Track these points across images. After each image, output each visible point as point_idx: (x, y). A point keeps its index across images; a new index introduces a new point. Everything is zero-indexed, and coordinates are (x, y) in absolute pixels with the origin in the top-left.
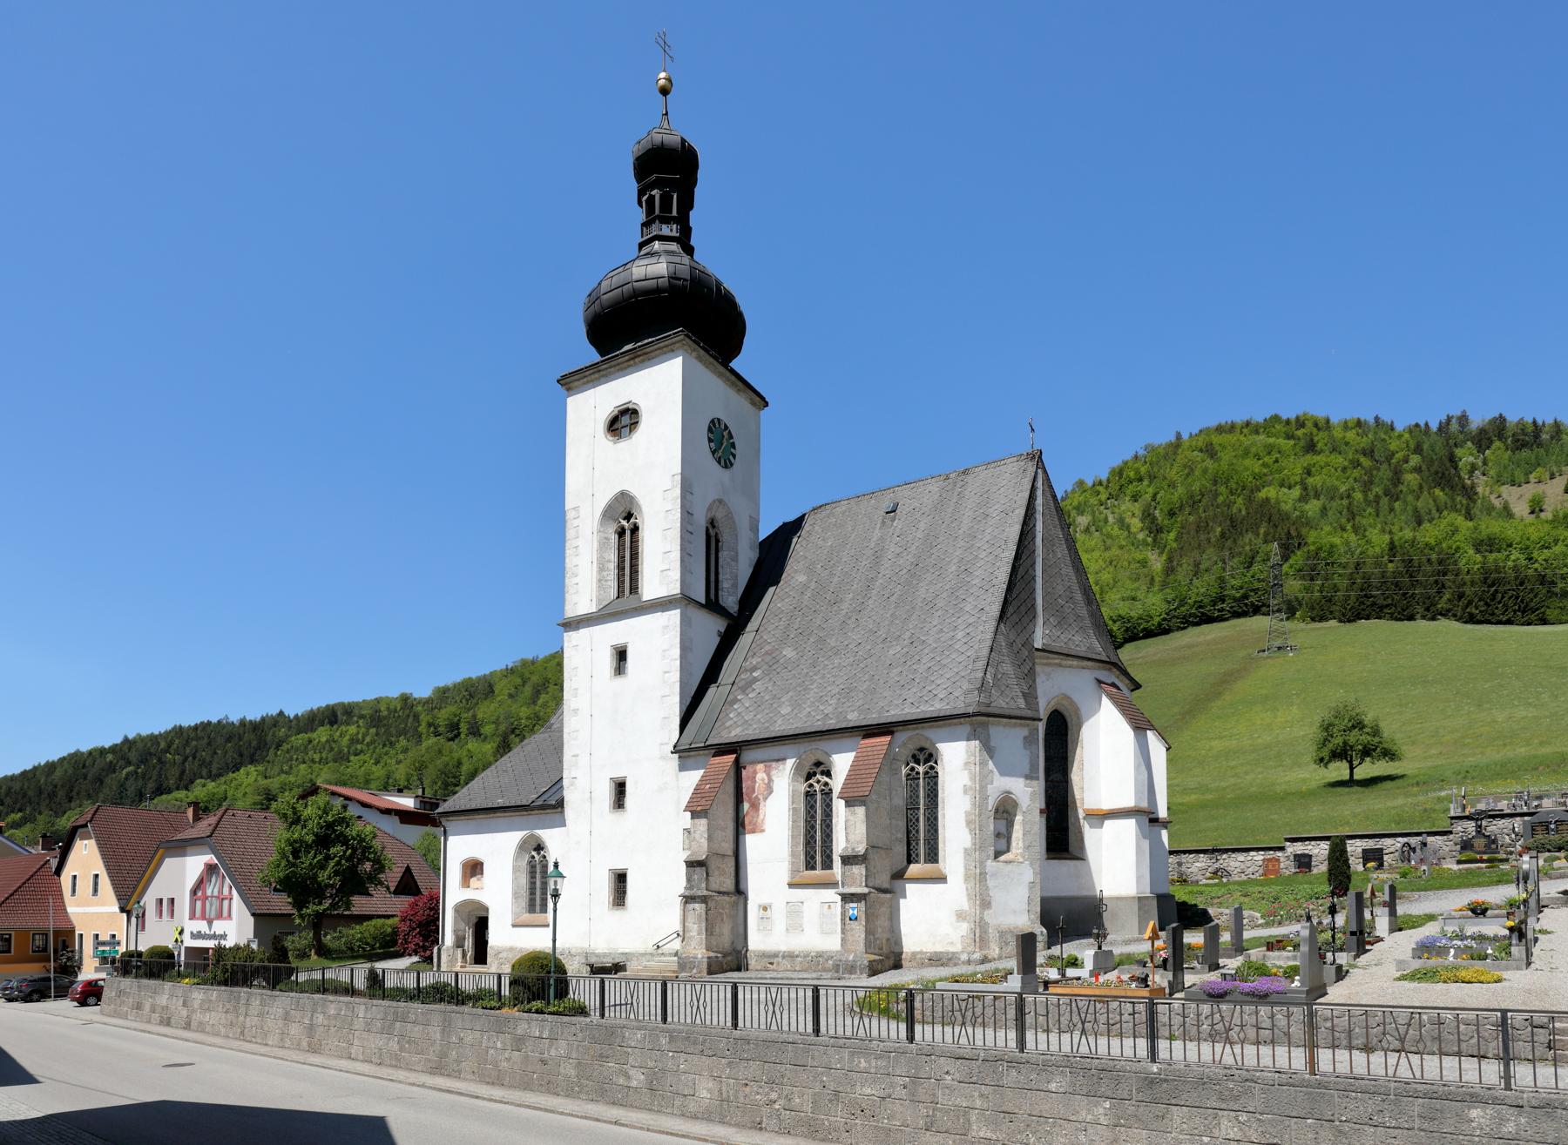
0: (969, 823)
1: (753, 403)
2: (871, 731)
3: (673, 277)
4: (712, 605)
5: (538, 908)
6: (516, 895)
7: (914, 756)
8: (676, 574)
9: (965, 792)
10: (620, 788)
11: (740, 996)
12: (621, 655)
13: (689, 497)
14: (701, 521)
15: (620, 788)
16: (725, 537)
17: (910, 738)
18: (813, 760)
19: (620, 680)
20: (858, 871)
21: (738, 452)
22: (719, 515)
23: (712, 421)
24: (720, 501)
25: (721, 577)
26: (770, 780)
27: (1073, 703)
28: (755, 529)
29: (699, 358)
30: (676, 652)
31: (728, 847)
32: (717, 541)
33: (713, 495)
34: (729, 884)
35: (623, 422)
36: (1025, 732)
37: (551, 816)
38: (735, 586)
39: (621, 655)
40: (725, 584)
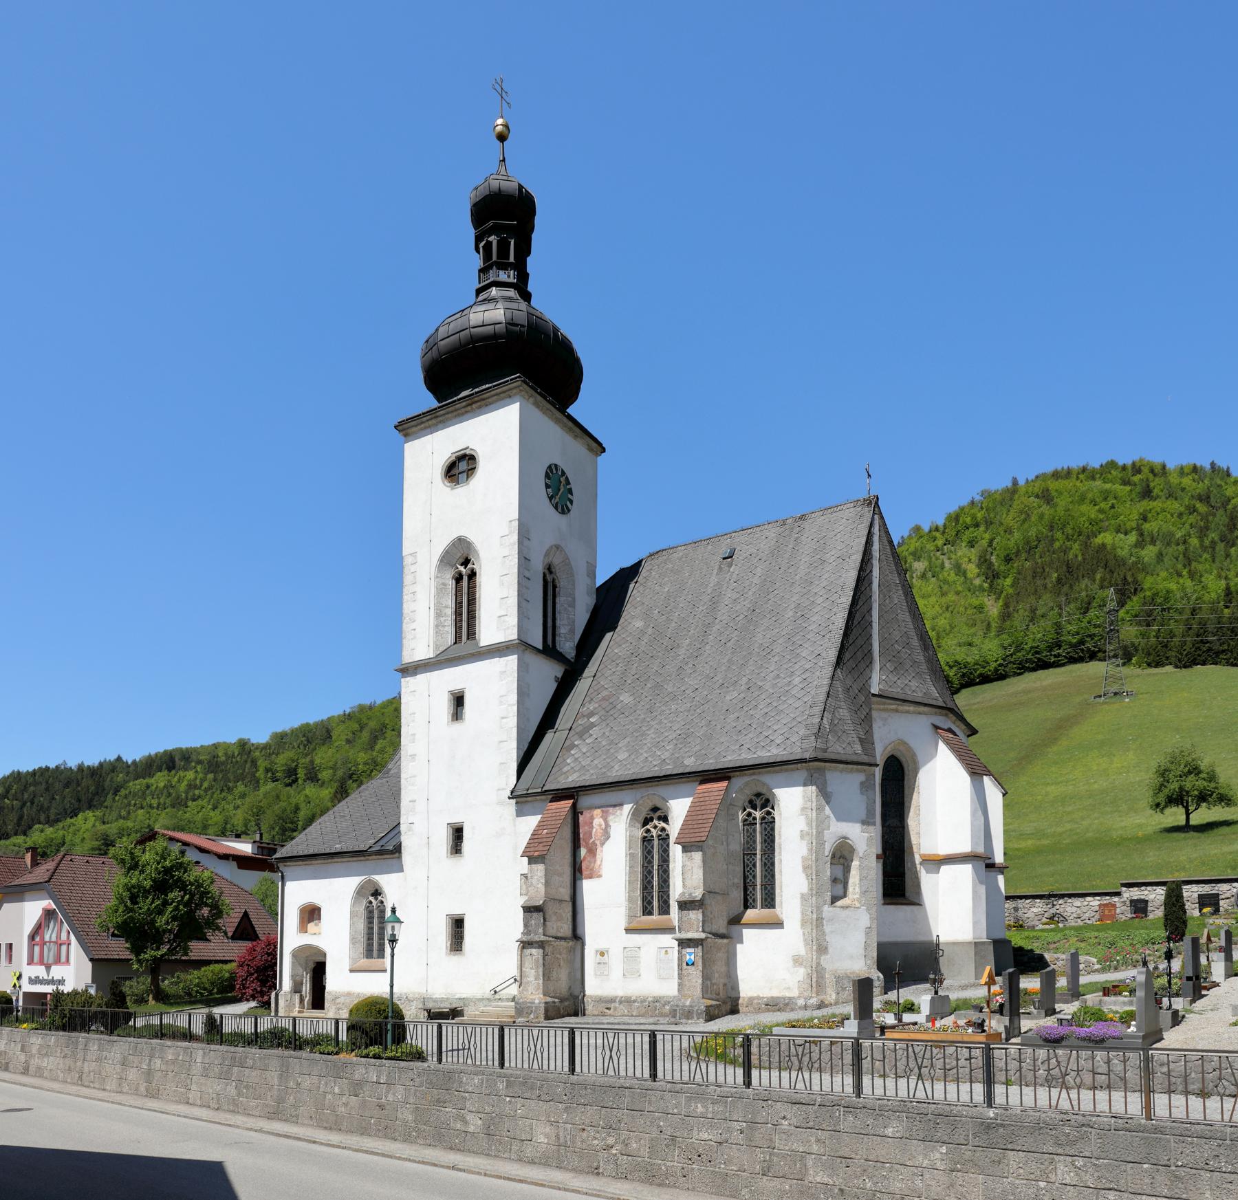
1: (590, 449)
3: (510, 323)
4: (550, 650)
7: (751, 802)
8: (513, 620)
9: (802, 837)
10: (457, 834)
13: (526, 542)
15: (457, 834)
16: (562, 583)
18: (650, 805)
19: (457, 726)
22: (557, 561)
23: (550, 467)
24: (558, 547)
25: (558, 622)
27: (909, 749)
29: (536, 404)
31: (565, 893)
32: (554, 587)
33: (549, 541)
34: (566, 930)
35: (460, 467)
36: (861, 777)
37: (389, 861)
38: (572, 631)
40: (562, 630)
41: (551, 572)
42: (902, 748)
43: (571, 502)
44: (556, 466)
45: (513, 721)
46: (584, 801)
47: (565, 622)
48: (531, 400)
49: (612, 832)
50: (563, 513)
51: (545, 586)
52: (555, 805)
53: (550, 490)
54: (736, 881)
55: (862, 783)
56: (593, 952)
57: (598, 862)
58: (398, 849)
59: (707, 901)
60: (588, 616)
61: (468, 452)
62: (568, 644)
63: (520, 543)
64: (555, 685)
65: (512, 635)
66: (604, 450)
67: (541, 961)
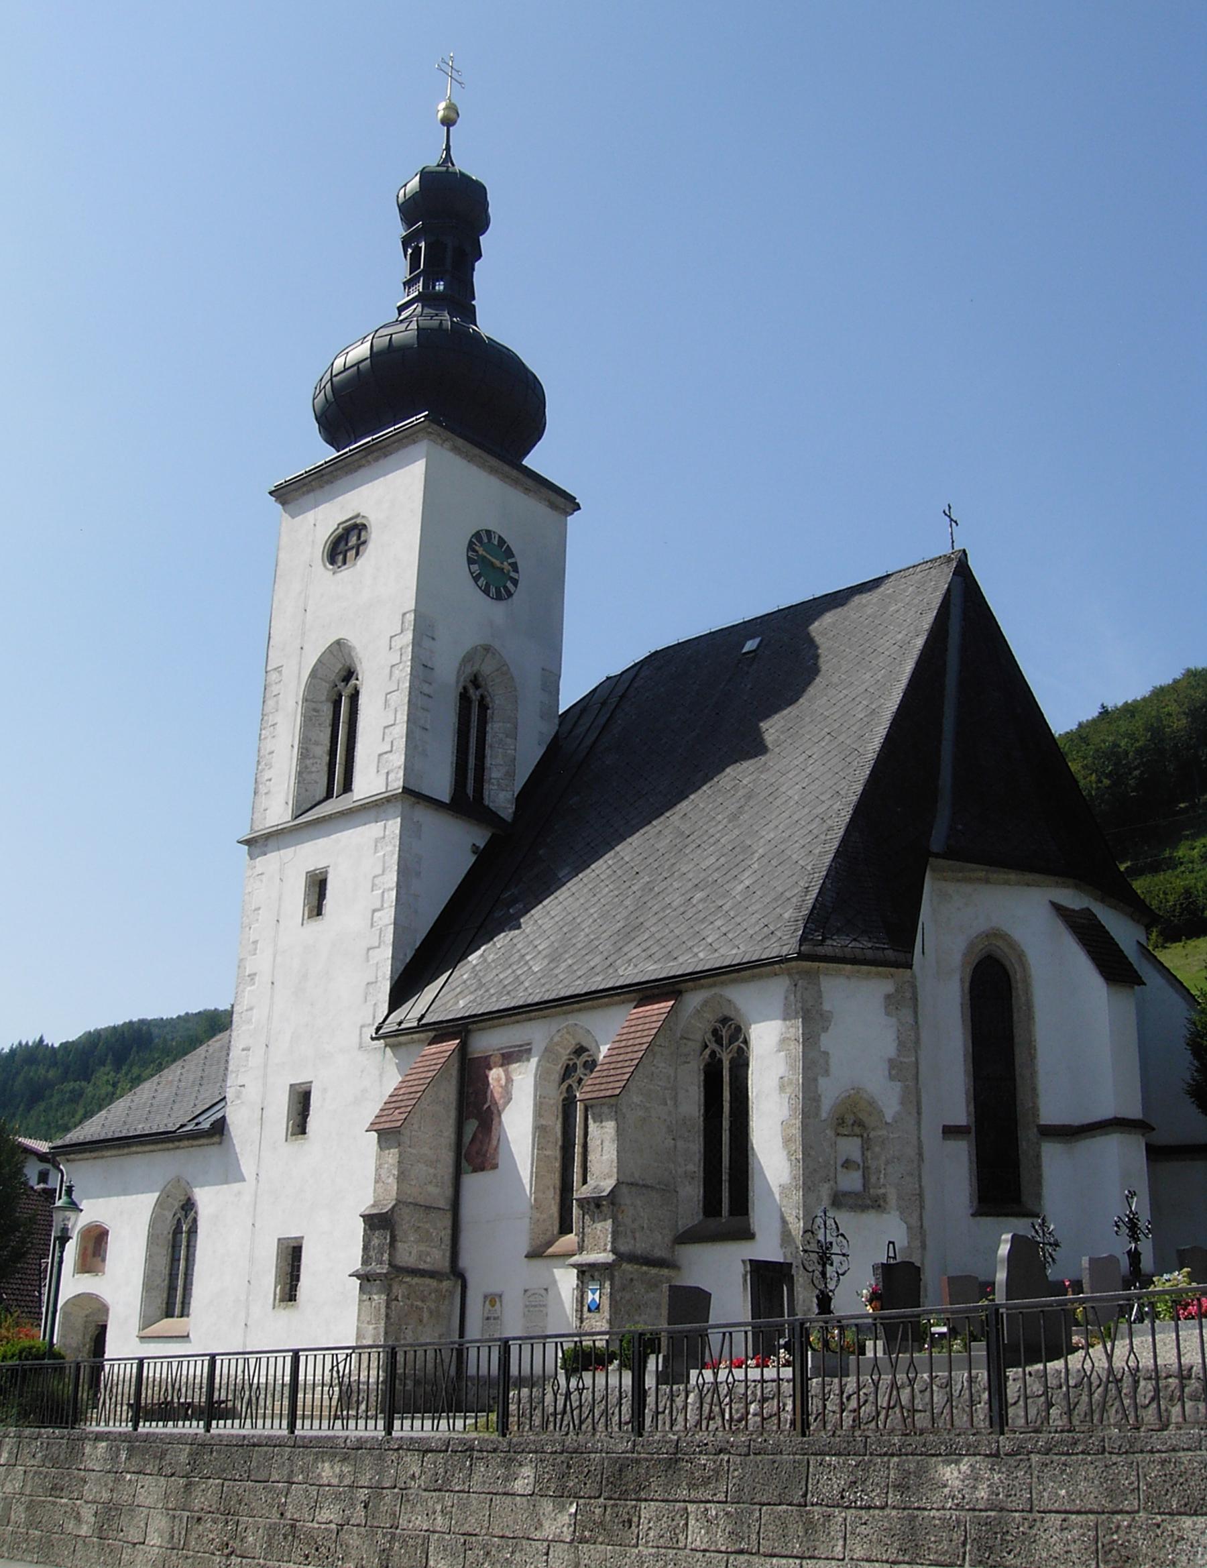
0: (787, 1141)
1: (553, 506)
2: (646, 992)
3: (373, 354)
4: (466, 801)
5: (177, 1311)
6: (148, 1286)
7: (715, 1032)
8: (398, 759)
9: (782, 1088)
10: (302, 1101)
11: (286, 1402)
12: (318, 886)
13: (427, 643)
14: (448, 673)
15: (302, 1101)
16: (498, 700)
17: (706, 1003)
18: (572, 1044)
19: (316, 925)
20: (603, 1229)
21: (522, 577)
22: (487, 668)
23: (477, 535)
24: (487, 649)
25: (488, 761)
26: (509, 1080)
27: (1013, 945)
28: (551, 683)
29: (455, 449)
30: (392, 878)
31: (439, 1194)
32: (484, 707)
33: (470, 641)
34: (437, 1258)
35: (345, 544)
36: (888, 987)
37: (210, 1153)
38: (511, 775)
39: (318, 886)
40: (495, 772)
41: (477, 687)
42: (1000, 943)
43: (515, 582)
44: (488, 532)
45: (387, 916)
46: (486, 1042)
47: (500, 761)
48: (447, 445)
49: (515, 1093)
50: (499, 597)
51: (465, 708)
52: (434, 1048)
53: (475, 567)
54: (691, 1167)
55: (888, 997)
56: (480, 1300)
57: (494, 1143)
58: (220, 1128)
59: (626, 1198)
60: (540, 752)
61: (359, 521)
62: (502, 795)
63: (416, 643)
64: (473, 859)
65: (397, 784)
66: (578, 507)
67: (383, 1310)
